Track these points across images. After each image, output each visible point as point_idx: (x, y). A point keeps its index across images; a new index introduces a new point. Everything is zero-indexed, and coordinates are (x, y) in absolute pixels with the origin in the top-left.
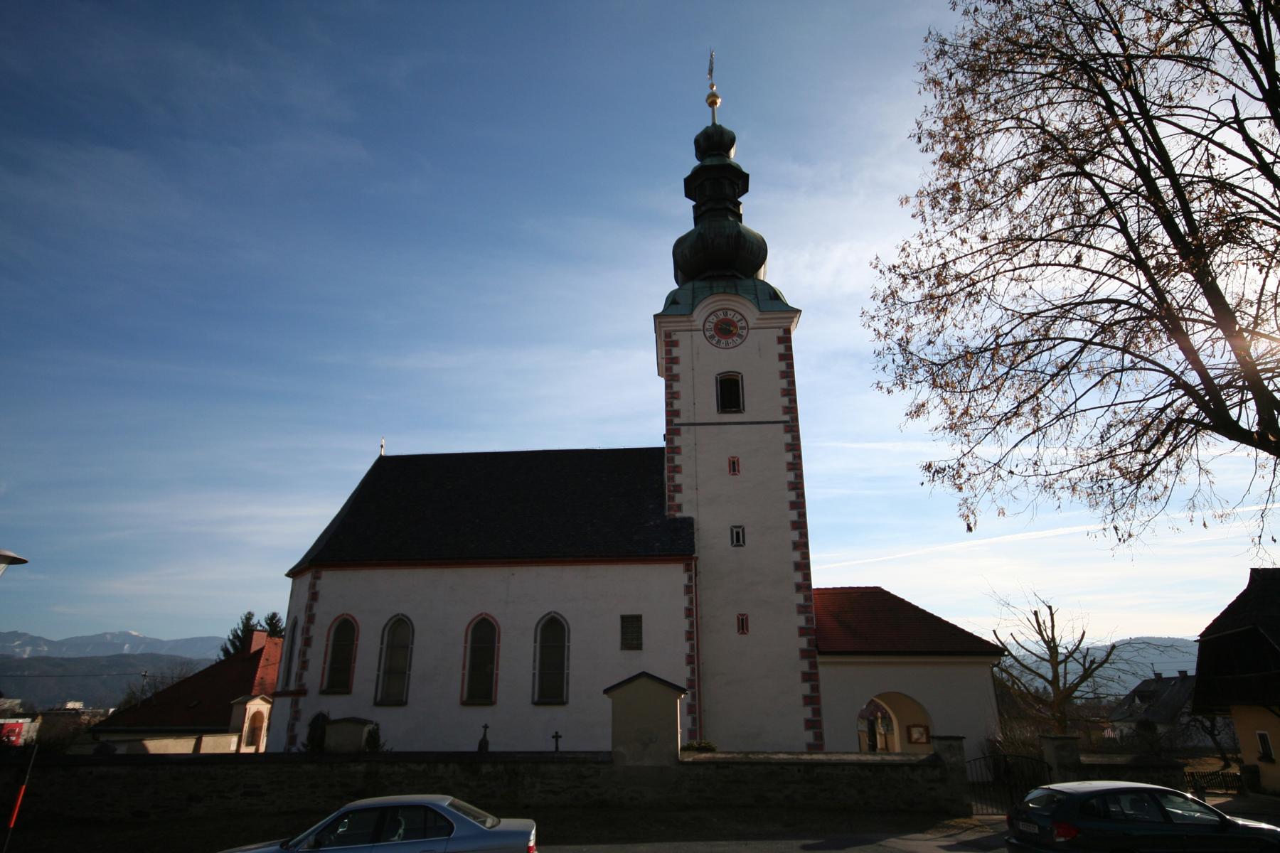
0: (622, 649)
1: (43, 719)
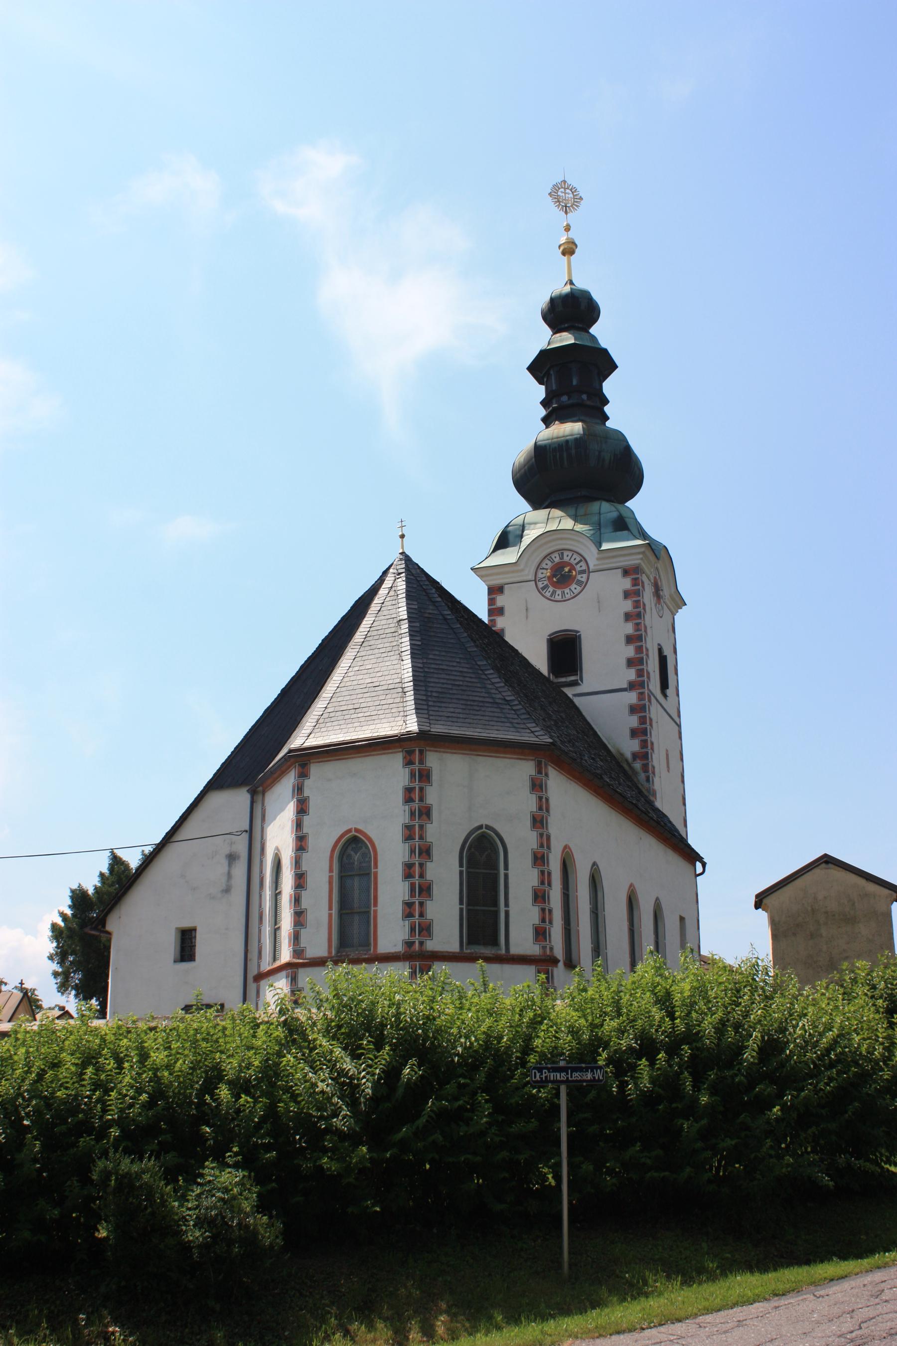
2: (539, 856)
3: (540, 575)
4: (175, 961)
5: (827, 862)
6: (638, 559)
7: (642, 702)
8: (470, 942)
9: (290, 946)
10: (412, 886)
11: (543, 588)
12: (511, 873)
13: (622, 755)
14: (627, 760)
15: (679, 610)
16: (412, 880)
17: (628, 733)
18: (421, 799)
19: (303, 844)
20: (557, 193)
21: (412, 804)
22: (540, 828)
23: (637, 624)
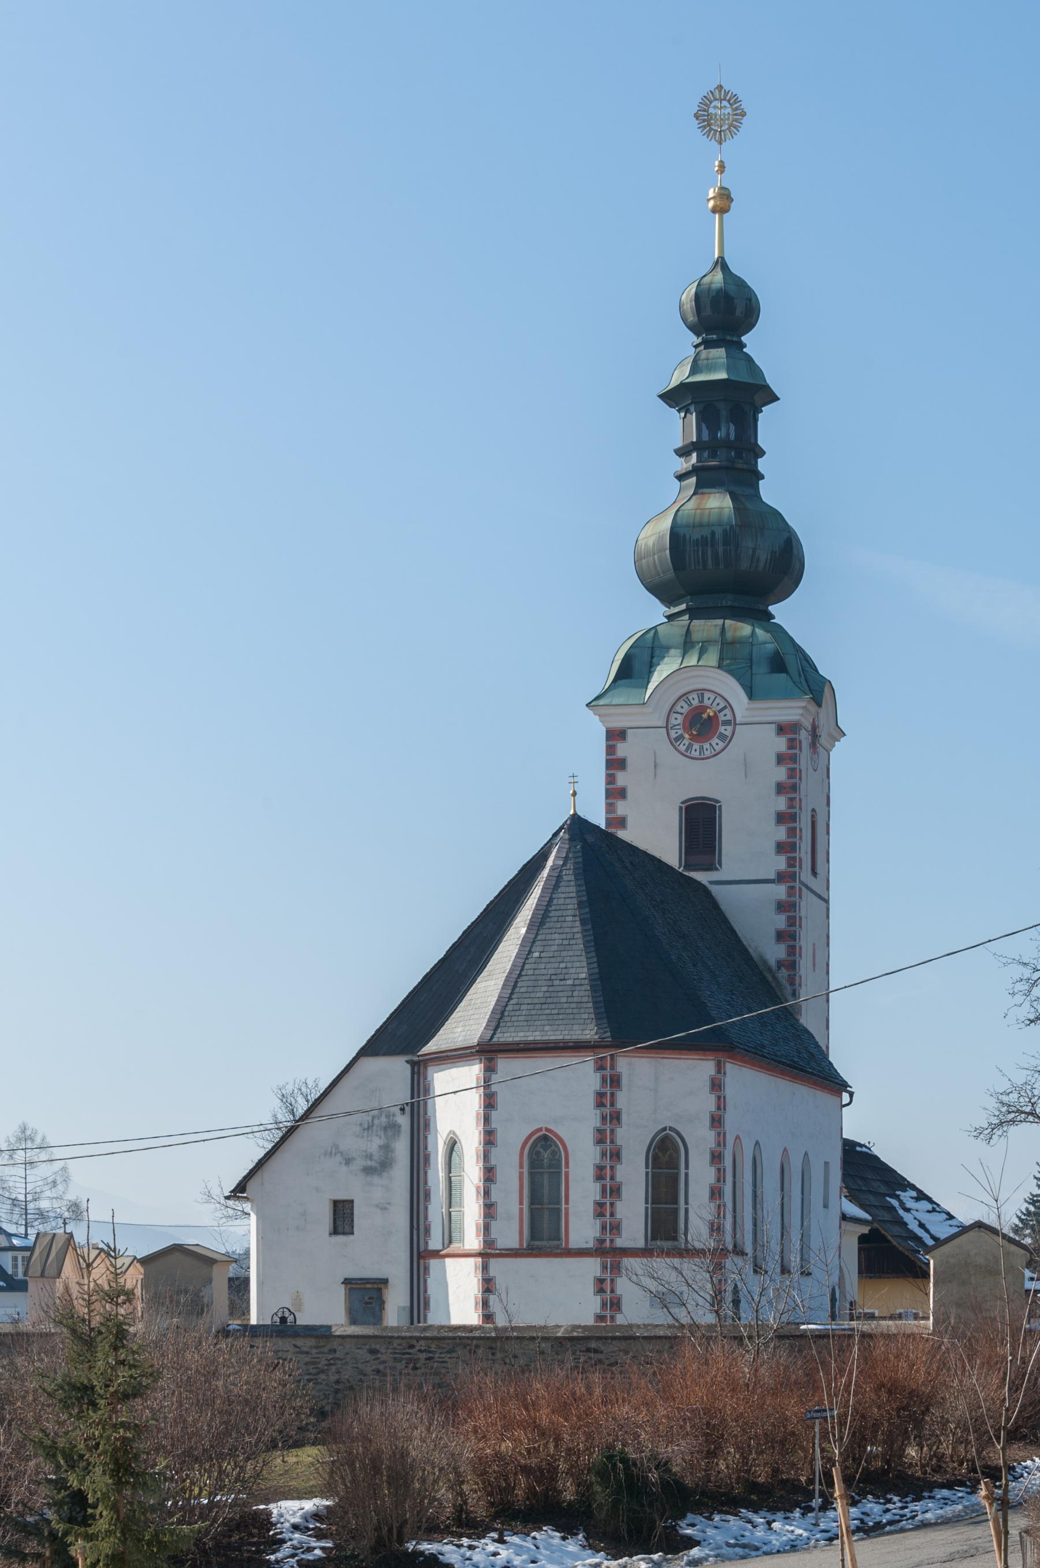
0: (352, 1201)
1: (324, 1558)
2: (716, 1154)
3: (673, 722)
4: (330, 1234)
5: (980, 1227)
6: (796, 715)
7: (792, 899)
8: (654, 1238)
9: (478, 1235)
11: (677, 739)
12: (691, 1171)
13: (765, 962)
14: (770, 969)
15: (836, 743)
16: (604, 1182)
17: (773, 934)
18: (612, 1104)
19: (492, 1138)
20: (708, 111)
21: (603, 1109)
22: (717, 1127)
23: (791, 800)
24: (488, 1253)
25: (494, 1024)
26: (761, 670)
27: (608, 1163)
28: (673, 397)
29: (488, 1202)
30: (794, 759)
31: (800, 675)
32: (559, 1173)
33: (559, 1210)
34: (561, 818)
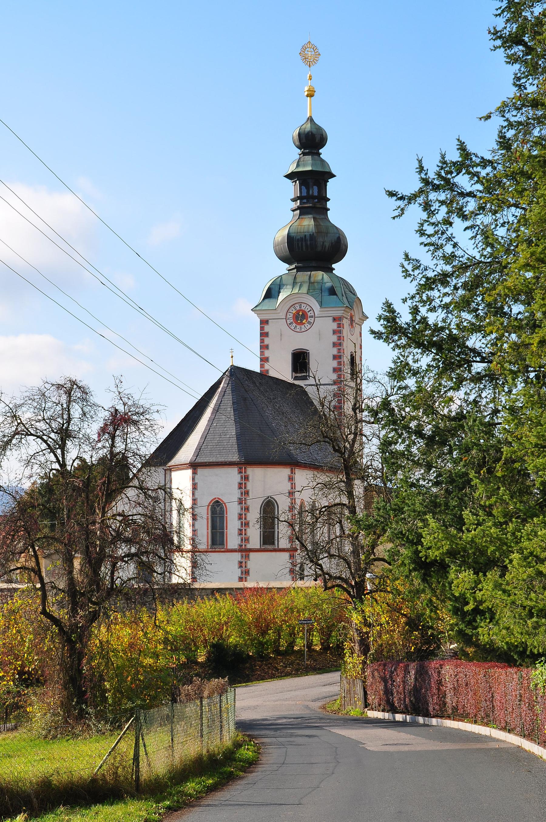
3: (288, 316)
10: (242, 523)
11: (290, 324)
16: (242, 520)
18: (245, 488)
23: (339, 349)
24: (194, 551)
25: (196, 454)
26: (326, 294)
27: (243, 512)
28: (290, 176)
29: (194, 529)
30: (340, 332)
31: (343, 295)
32: (223, 517)
33: (223, 532)
34: (225, 367)
